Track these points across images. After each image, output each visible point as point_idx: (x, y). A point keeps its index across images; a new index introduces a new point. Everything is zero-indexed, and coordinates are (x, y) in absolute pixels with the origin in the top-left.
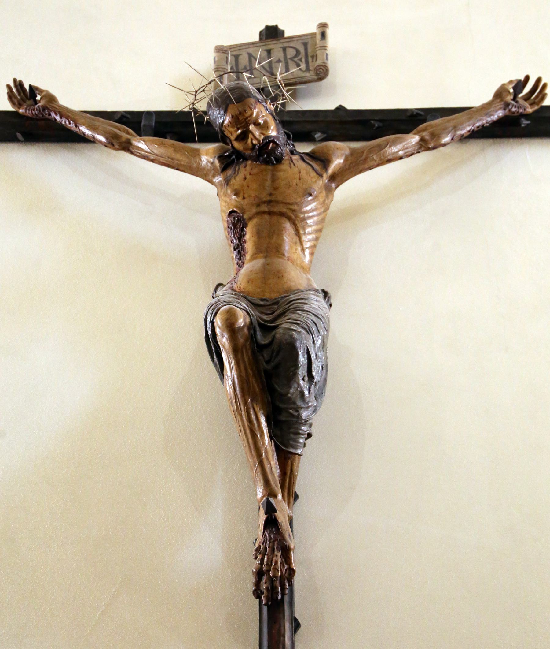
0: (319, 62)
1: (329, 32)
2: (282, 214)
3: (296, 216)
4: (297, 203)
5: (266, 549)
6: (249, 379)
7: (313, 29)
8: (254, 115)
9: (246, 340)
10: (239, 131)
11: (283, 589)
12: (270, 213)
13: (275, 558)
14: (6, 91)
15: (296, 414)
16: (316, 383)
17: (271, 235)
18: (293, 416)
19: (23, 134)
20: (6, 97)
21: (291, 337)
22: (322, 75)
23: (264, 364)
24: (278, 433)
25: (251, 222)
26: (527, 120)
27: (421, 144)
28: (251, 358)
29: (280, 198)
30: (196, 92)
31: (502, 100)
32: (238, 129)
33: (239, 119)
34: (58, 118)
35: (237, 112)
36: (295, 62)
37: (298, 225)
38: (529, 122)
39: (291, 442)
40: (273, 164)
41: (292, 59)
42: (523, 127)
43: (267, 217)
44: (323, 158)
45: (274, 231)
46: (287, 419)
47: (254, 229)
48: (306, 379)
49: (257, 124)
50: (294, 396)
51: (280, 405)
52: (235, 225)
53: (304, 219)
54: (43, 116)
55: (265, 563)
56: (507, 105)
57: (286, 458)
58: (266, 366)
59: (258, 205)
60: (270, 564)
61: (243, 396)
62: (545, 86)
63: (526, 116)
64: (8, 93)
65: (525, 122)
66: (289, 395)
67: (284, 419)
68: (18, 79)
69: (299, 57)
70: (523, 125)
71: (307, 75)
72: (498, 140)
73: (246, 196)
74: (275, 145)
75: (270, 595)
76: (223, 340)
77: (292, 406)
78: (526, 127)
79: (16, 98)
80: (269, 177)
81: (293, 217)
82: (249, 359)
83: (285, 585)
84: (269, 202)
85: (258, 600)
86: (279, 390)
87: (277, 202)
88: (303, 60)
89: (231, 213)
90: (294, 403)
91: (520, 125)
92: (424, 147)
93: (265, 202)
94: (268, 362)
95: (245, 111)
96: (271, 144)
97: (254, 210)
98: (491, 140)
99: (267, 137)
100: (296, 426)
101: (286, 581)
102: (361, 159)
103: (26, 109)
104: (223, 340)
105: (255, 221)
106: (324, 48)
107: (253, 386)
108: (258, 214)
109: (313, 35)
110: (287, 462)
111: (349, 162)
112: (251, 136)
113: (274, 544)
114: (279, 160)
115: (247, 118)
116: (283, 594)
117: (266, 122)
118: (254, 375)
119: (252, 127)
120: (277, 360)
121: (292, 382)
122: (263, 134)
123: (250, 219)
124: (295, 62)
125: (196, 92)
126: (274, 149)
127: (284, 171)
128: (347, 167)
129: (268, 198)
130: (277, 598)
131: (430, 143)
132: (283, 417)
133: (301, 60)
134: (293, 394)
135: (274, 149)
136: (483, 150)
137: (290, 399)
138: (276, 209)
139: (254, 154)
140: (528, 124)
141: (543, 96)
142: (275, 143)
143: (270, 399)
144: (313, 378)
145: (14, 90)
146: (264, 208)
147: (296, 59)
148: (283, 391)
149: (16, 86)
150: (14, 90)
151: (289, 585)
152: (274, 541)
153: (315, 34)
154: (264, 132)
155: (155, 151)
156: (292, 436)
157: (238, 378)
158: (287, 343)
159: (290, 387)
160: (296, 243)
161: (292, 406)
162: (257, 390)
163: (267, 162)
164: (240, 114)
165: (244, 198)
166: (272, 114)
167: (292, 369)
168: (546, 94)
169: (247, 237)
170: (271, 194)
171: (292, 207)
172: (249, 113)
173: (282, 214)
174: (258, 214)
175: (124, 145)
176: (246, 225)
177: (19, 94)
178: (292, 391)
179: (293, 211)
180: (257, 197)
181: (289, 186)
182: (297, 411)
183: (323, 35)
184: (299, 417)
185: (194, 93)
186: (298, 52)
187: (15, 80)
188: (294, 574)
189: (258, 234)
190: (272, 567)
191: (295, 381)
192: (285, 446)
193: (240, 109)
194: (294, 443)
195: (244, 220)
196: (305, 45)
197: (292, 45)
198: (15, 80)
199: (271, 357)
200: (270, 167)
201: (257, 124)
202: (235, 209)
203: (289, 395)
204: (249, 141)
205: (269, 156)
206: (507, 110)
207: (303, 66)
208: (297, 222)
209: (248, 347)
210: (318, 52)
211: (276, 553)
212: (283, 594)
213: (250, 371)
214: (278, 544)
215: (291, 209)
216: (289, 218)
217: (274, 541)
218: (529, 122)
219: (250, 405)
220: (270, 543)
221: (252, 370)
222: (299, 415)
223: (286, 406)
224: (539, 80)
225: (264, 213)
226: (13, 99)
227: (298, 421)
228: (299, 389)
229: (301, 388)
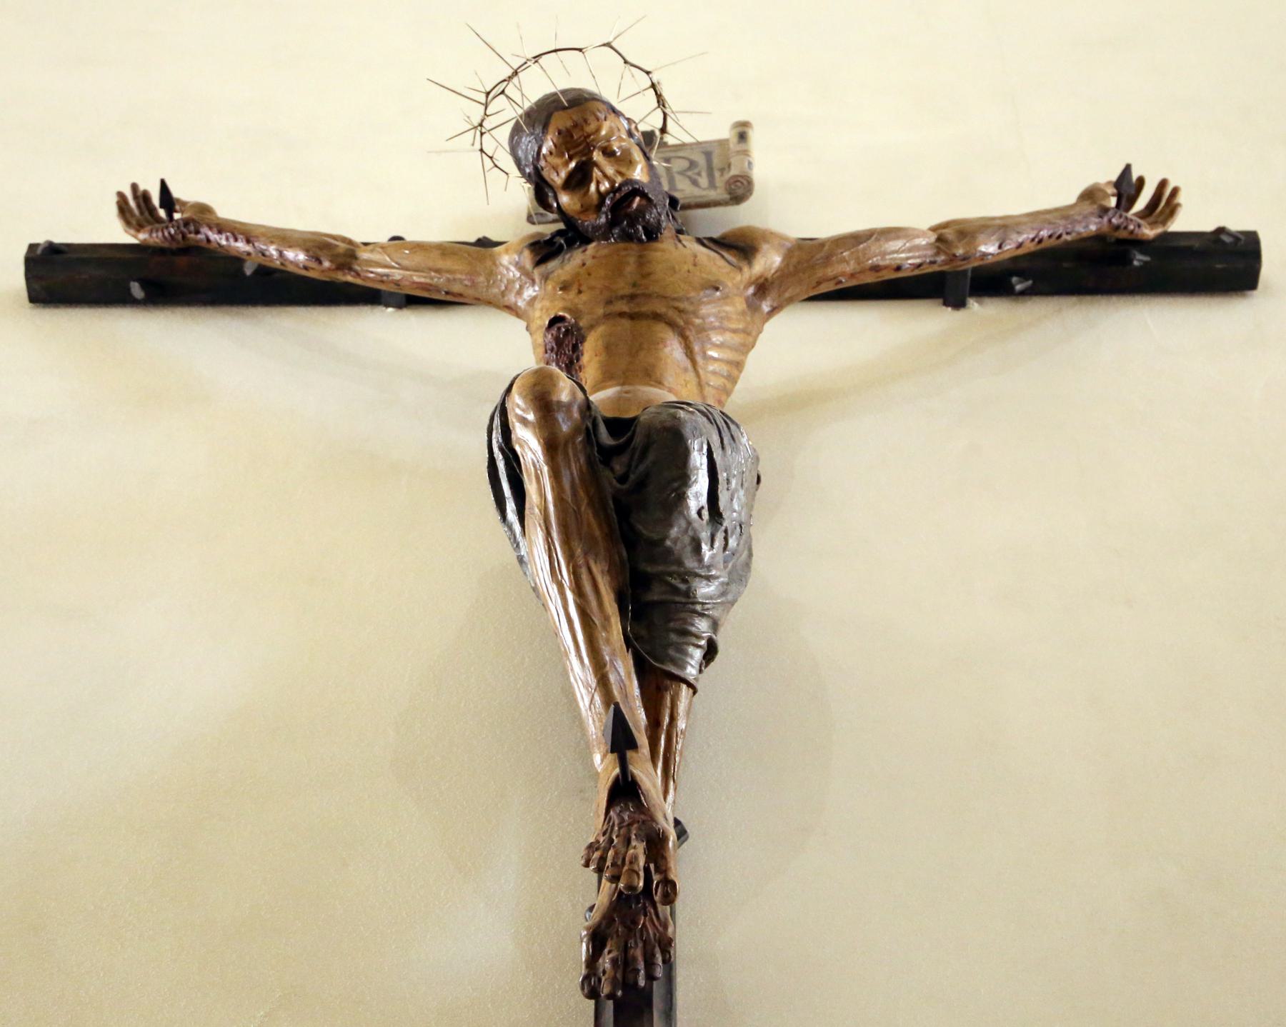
0: (734, 172)
1: (754, 136)
2: (657, 317)
3: (687, 322)
4: (688, 299)
5: (611, 841)
6: (579, 509)
7: (722, 131)
8: (603, 133)
9: (576, 431)
10: (573, 165)
11: (650, 964)
12: (633, 317)
13: (631, 851)
14: (115, 199)
15: (683, 587)
16: (726, 531)
17: (634, 353)
18: (676, 590)
19: (145, 284)
20: (114, 210)
21: (674, 417)
22: (740, 192)
23: (614, 482)
24: (643, 632)
25: (593, 333)
26: (1143, 253)
27: (938, 248)
28: (584, 468)
29: (654, 288)
30: (488, 94)
31: (1094, 202)
32: (571, 158)
33: (572, 136)
34: (214, 236)
35: (569, 124)
36: (690, 178)
37: (691, 338)
38: (1147, 259)
39: (671, 652)
40: (640, 240)
41: (682, 173)
42: (1136, 268)
43: (626, 323)
44: (742, 244)
45: (641, 345)
46: (664, 597)
47: (600, 343)
48: (705, 513)
49: (608, 153)
50: (679, 545)
51: (649, 569)
52: (559, 342)
53: (701, 330)
54: (184, 237)
55: (609, 863)
56: (1105, 210)
57: (658, 680)
58: (618, 486)
59: (609, 302)
60: (619, 863)
61: (566, 542)
62: (1175, 191)
63: (1141, 244)
64: (118, 203)
65: (1139, 259)
66: (668, 543)
67: (655, 598)
68: (142, 187)
69: (696, 171)
70: (1136, 263)
71: (713, 195)
72: (1088, 298)
73: (583, 288)
74: (644, 202)
75: (619, 976)
76: (530, 445)
77: (674, 568)
78: (1141, 268)
79: (132, 214)
80: (632, 260)
81: (682, 323)
82: (581, 470)
83: (653, 955)
84: (632, 297)
85: (592, 1002)
86: (644, 532)
87: (648, 296)
88: (704, 174)
89: (555, 321)
90: (680, 563)
91: (1131, 261)
92: (946, 253)
93: (622, 297)
94: (623, 479)
95: (586, 121)
96: (638, 199)
97: (600, 311)
98: (1074, 299)
99: (629, 182)
100: (683, 615)
101: (657, 950)
102: (818, 256)
103: (151, 232)
104: (530, 445)
105: (601, 329)
106: (746, 153)
107: (589, 525)
108: (607, 316)
109: (722, 143)
110: (662, 698)
111: (794, 260)
112: (596, 173)
113: (629, 831)
114: (653, 233)
115: (589, 136)
116: (651, 977)
117: (627, 153)
118: (591, 503)
119: (597, 156)
120: (642, 468)
121: (676, 514)
122: (620, 173)
123: (592, 327)
124: (690, 178)
125: (488, 94)
126: (641, 211)
127: (663, 251)
128: (791, 268)
129: (628, 291)
130: (636, 983)
131: (957, 247)
132: (655, 594)
133: (699, 174)
134: (675, 541)
135: (641, 211)
136: (1060, 310)
137: (669, 551)
138: (644, 309)
139: (603, 220)
140: (1146, 263)
141: (1172, 209)
142: (644, 196)
143: (625, 554)
144: (720, 515)
145: (132, 203)
146: (623, 306)
147: (689, 173)
148: (655, 536)
149: (135, 197)
150: (132, 203)
151: (664, 962)
152: (630, 825)
153: (727, 140)
154: (623, 170)
155: (406, 263)
156: (673, 637)
157: (555, 506)
158: (666, 429)
159: (671, 526)
160: (686, 370)
161: (674, 568)
162: (597, 533)
163: (628, 237)
164: (576, 126)
165: (580, 292)
166: (638, 145)
167: (676, 485)
168: (1178, 205)
169: (585, 359)
170: (634, 285)
171: (677, 304)
172: (592, 127)
173: (657, 317)
174: (607, 316)
175: (341, 260)
176: (582, 339)
177: (142, 213)
178: (674, 532)
179: (681, 311)
180: (607, 288)
181: (673, 270)
182: (685, 581)
183: (742, 137)
184: (689, 594)
185: (482, 98)
186: (693, 164)
187: (134, 187)
188: (675, 894)
189: (609, 348)
190: (626, 868)
191: (681, 513)
192: (656, 660)
193: (575, 117)
194: (678, 655)
195: (579, 329)
196: (708, 155)
197: (681, 154)
198: (134, 187)
199: (629, 466)
200: (634, 246)
201: (608, 153)
202: (561, 314)
203: (668, 543)
204: (593, 187)
205: (632, 224)
206: (1106, 219)
207: (704, 181)
208: (688, 333)
209: (579, 447)
210: (733, 161)
211: (634, 843)
212: (651, 977)
213: (582, 493)
214: (639, 829)
215: (676, 308)
216: (672, 325)
217: (630, 825)
218: (1147, 259)
219: (581, 561)
220: (620, 828)
221: (587, 493)
222: (689, 588)
223: (660, 568)
224: (1163, 184)
225: (621, 315)
226: (128, 215)
227: (685, 604)
228: (690, 533)
229: (695, 530)
